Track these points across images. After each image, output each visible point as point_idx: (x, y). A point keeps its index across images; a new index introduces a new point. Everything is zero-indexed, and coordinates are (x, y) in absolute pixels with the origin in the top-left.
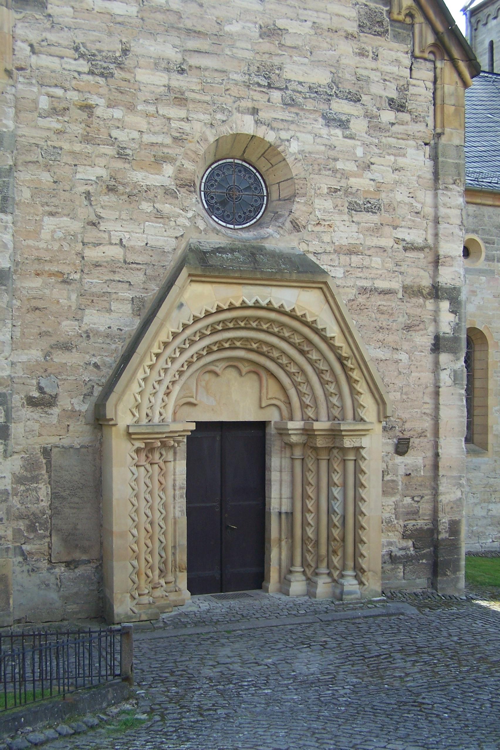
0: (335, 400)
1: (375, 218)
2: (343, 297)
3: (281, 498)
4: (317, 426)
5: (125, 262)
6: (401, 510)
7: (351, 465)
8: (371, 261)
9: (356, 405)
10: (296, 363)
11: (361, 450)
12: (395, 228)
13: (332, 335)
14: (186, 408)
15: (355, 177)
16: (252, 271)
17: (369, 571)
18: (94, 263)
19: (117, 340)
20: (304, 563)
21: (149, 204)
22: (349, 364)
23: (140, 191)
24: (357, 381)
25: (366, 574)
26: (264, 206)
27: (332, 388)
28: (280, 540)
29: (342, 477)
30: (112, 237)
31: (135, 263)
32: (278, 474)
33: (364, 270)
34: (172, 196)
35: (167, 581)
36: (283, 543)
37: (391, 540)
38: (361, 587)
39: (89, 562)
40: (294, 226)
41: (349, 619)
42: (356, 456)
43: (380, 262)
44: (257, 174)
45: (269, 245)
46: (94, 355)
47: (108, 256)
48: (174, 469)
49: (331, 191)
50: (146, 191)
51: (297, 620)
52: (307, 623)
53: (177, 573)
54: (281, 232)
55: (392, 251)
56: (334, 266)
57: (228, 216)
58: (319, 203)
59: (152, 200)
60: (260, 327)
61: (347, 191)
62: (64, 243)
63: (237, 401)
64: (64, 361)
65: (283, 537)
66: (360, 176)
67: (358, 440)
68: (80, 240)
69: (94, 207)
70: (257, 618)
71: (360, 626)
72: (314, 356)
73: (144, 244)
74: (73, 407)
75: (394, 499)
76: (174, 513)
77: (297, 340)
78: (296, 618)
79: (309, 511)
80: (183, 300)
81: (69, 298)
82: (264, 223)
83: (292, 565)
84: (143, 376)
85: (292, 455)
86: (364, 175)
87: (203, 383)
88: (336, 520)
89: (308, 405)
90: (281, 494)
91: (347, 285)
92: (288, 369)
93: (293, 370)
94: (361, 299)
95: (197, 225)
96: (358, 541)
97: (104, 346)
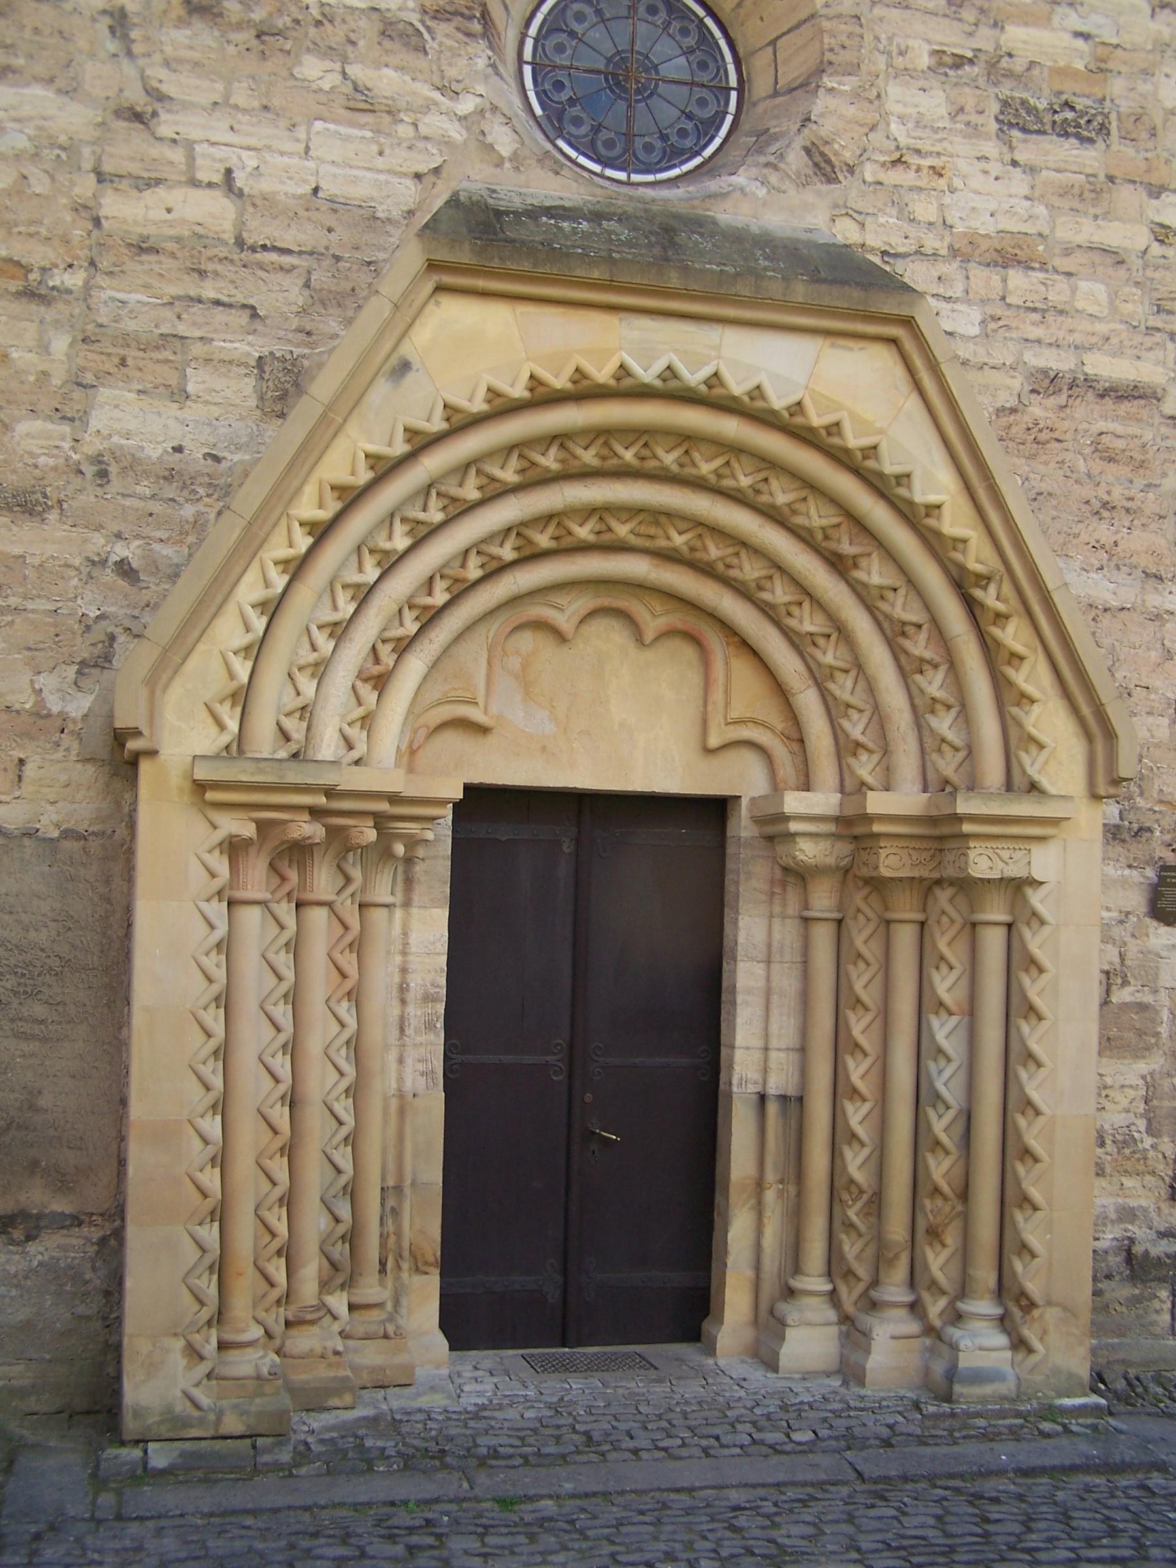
0: (944, 724)
1: (1091, 158)
2: (980, 399)
3: (766, 1049)
4: (876, 803)
5: (240, 243)
6: (1166, 1103)
7: (993, 942)
8: (1074, 290)
9: (1016, 741)
10: (818, 604)
11: (1029, 891)
12: (1156, 191)
13: (933, 498)
14: (452, 740)
15: (1026, 24)
16: (649, 264)
17: (1049, 1303)
18: (134, 240)
19: (202, 491)
20: (835, 1266)
21: (328, 64)
22: (989, 597)
23: (297, 22)
24: (1016, 658)
25: (1036, 1313)
26: (729, 119)
27: (934, 684)
28: (760, 1185)
29: (964, 982)
30: (199, 162)
31: (275, 249)
32: (760, 970)
33: (1050, 317)
34: (406, 45)
35: (357, 1300)
36: (770, 1196)
37: (1133, 1203)
38: (1020, 1356)
39: (76, 1221)
40: (816, 165)
41: (961, 1476)
42: (1012, 913)
43: (1103, 297)
44: (709, 22)
45: (728, 215)
46: (119, 536)
47: (184, 221)
48: (405, 934)
49: (941, 64)
50: (318, 23)
51: (776, 1469)
52: (804, 1484)
53: (405, 1275)
54: (774, 178)
55: (1145, 266)
56: (948, 299)
57: (610, 144)
58: (900, 98)
59: (339, 54)
60: (689, 471)
61: (996, 67)
62: (32, 170)
63: (622, 725)
64: (17, 550)
65: (770, 1176)
66: (1044, 21)
67: (1018, 855)
68: (87, 165)
69: (141, 62)
70: (636, 1452)
71: (994, 1511)
72: (875, 574)
73: (308, 189)
74: (40, 702)
75: (1142, 1067)
76: (400, 1079)
77: (817, 516)
78: (775, 1459)
79: (855, 1093)
80: (407, 350)
81: (44, 348)
82: (724, 166)
83: (797, 1270)
84: (259, 594)
85: (806, 907)
86: (1056, 20)
87: (515, 663)
88: (940, 1124)
89: (858, 744)
90: (766, 1036)
91: (992, 362)
92: (792, 623)
93: (808, 627)
94: (1039, 410)
95: (489, 139)
96: (1011, 1199)
97: (156, 507)
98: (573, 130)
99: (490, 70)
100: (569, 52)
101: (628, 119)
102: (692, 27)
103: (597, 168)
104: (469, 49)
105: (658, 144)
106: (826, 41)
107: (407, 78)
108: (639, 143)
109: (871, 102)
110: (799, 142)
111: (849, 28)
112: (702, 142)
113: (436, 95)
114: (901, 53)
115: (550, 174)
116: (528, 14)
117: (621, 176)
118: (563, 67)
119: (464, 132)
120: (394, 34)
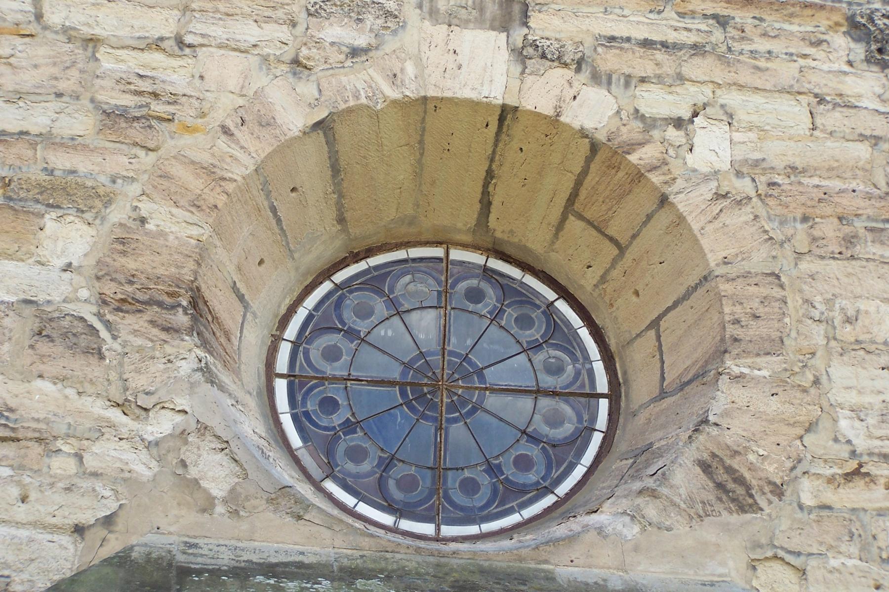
26: (597, 439)
40: (720, 486)
44: (562, 306)
54: (651, 511)
95: (193, 472)
98: (350, 466)
99: (198, 376)
100: (346, 358)
101: (437, 448)
102: (536, 314)
103: (387, 519)
104: (168, 349)
105: (485, 480)
106: (727, 310)
107: (71, 392)
108: (453, 481)
109: (805, 391)
110: (690, 455)
111: (764, 291)
112: (555, 474)
113: (115, 415)
114: (848, 321)
115: (288, 519)
116: (283, 310)
117: (428, 529)
118: (335, 379)
119: (154, 464)
120: (54, 335)
